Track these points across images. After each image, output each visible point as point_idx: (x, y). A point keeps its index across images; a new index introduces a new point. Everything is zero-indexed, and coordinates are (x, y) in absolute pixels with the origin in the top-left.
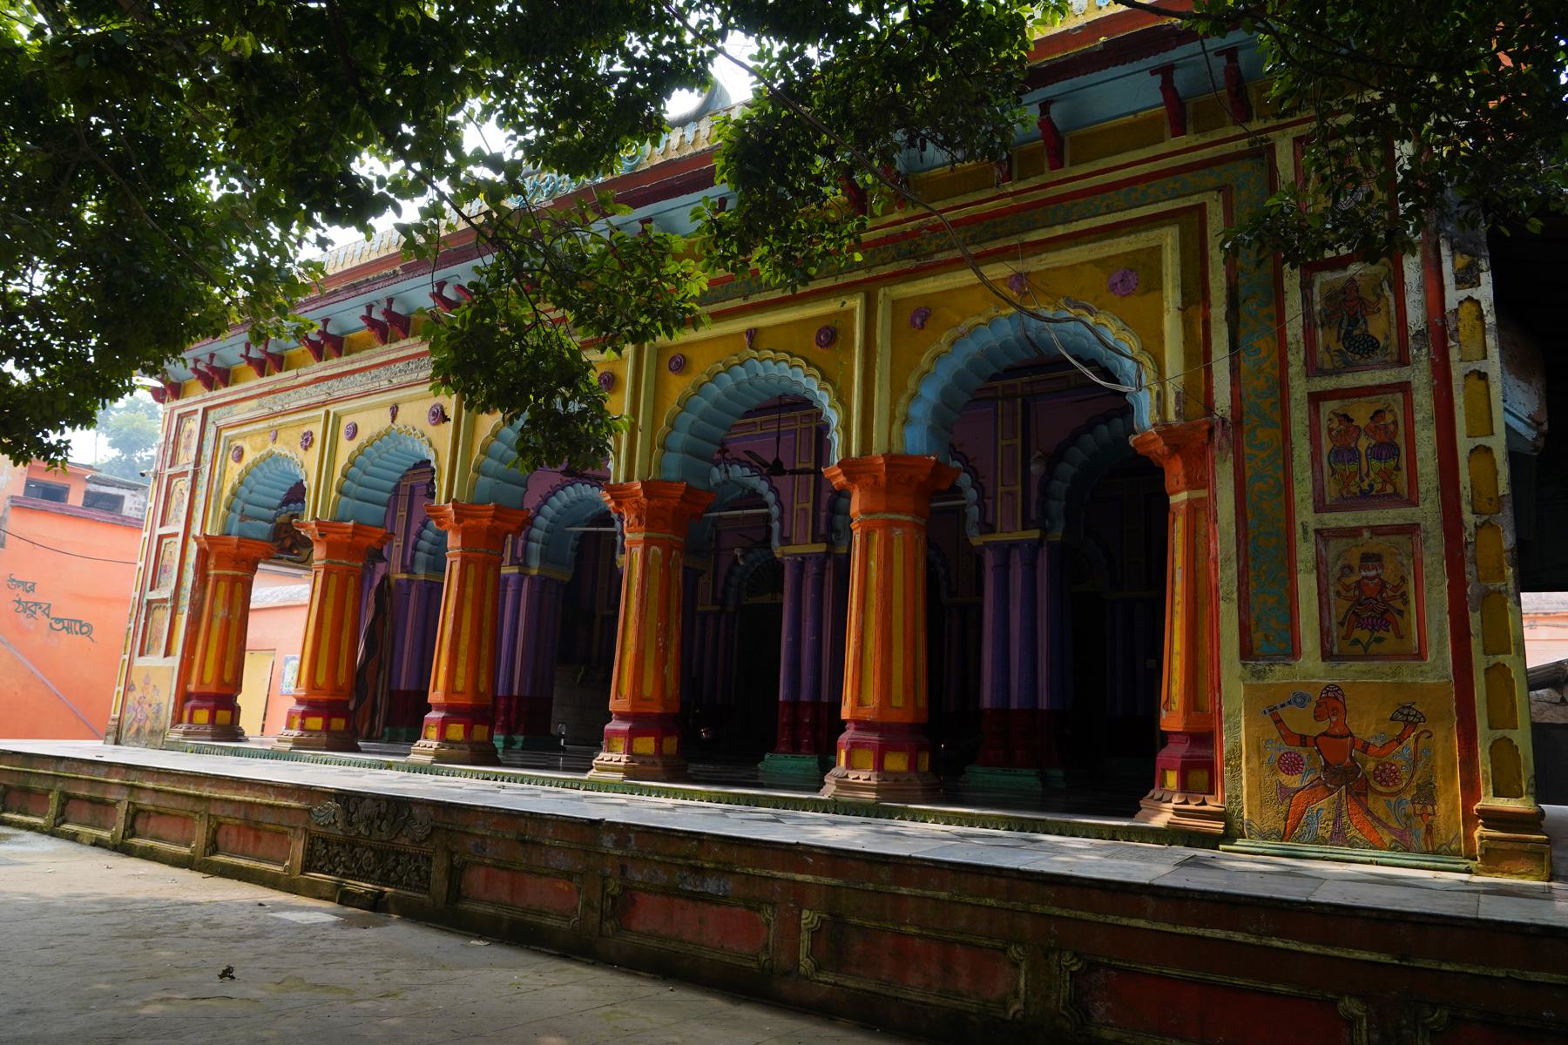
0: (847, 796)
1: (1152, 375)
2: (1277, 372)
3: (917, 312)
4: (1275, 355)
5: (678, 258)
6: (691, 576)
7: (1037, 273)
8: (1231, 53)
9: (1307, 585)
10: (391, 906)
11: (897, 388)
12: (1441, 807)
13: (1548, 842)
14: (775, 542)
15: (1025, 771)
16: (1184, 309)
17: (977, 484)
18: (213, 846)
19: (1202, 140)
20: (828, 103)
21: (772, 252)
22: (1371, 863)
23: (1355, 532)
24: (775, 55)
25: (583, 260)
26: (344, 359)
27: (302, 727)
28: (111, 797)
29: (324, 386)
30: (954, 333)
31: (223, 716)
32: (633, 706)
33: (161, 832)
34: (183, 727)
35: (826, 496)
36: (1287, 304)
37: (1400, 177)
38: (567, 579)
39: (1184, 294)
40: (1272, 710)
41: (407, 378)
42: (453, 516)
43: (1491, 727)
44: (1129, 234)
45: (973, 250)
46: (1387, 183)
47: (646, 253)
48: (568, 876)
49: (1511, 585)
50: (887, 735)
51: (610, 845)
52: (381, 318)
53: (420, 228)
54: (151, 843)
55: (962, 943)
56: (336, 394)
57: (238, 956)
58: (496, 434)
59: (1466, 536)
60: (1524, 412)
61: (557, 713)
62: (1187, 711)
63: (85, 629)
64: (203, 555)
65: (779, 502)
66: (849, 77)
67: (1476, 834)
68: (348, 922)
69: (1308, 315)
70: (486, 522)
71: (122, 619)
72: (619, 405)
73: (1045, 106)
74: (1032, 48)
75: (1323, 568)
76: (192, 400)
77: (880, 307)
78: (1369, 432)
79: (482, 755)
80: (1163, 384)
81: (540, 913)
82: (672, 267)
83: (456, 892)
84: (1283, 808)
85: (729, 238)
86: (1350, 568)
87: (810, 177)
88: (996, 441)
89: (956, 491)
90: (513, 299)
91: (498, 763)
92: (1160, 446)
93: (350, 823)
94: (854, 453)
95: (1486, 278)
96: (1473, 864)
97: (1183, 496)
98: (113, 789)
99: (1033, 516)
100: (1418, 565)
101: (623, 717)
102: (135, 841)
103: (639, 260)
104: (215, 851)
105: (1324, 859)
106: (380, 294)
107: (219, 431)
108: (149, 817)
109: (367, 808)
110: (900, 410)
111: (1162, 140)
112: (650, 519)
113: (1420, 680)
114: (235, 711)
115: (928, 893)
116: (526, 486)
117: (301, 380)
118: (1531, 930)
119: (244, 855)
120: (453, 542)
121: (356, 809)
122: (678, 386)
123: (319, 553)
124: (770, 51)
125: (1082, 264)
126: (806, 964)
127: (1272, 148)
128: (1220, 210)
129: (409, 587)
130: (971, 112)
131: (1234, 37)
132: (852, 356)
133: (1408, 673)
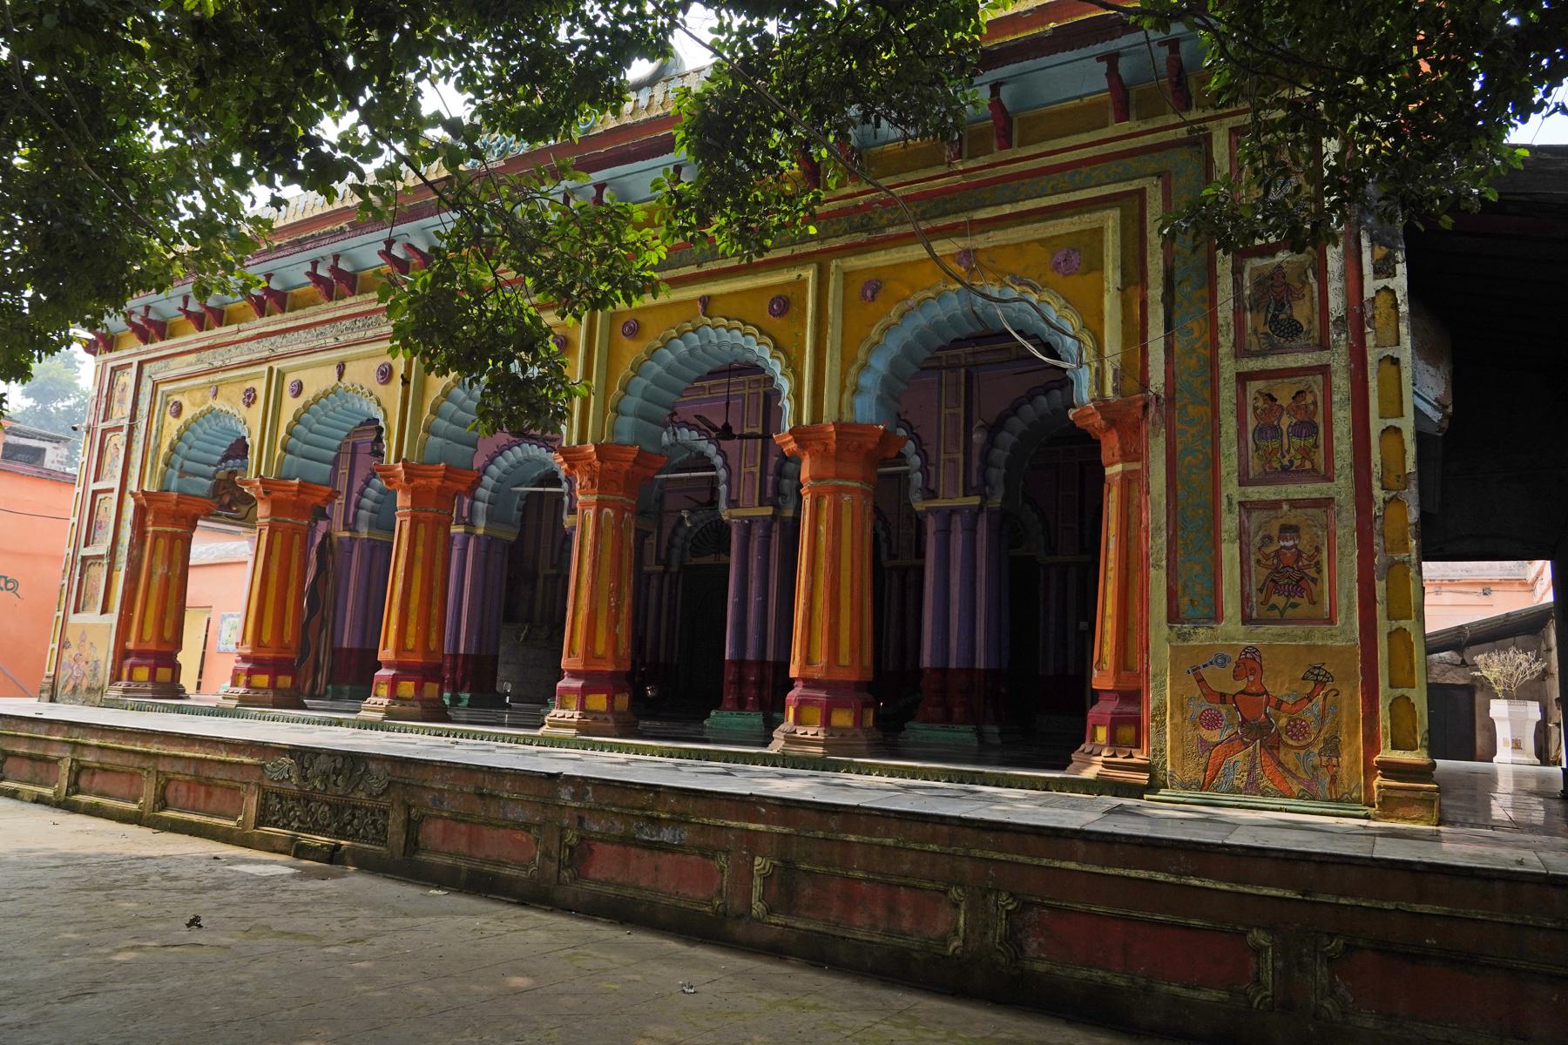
0: (796, 750)
1: (1092, 352)
2: (1207, 353)
3: (868, 284)
4: (1207, 337)
5: (638, 227)
6: (641, 536)
7: (985, 250)
8: (1174, 44)
9: (1230, 552)
10: (348, 859)
11: (847, 360)
12: (1345, 759)
13: (1438, 790)
14: (723, 505)
15: (962, 728)
16: (1122, 290)
17: (921, 451)
18: (162, 802)
19: (1144, 127)
20: (785, 78)
21: (729, 224)
22: (1280, 810)
23: (1275, 505)
24: (735, 29)
25: (543, 227)
26: (289, 315)
27: (248, 684)
28: (53, 754)
29: (266, 342)
30: (904, 306)
31: (164, 673)
32: (1117, 682)
33: (106, 789)
34: (123, 684)
35: (773, 460)
36: (1219, 287)
37: (1326, 173)
38: (513, 538)
39: (1123, 275)
40: (1195, 669)
41: (354, 336)
42: (403, 476)
43: (1391, 686)
44: (1072, 215)
45: (923, 226)
46: (1314, 176)
47: (604, 219)
48: (526, 827)
49: (1414, 556)
50: (835, 693)
52: (327, 275)
53: (377, 190)
54: (96, 799)
55: (906, 886)
56: (280, 351)
57: (202, 905)
58: (446, 394)
59: (1375, 510)
60: (1431, 395)
61: (502, 672)
62: (1117, 671)
63: (10, 585)
64: (140, 512)
65: (726, 465)
66: (807, 53)
67: (1375, 784)
68: (306, 874)
69: (1238, 299)
70: (436, 482)
71: (55, 576)
72: (575, 369)
73: (995, 88)
74: (985, 31)
75: (1245, 538)
76: (126, 352)
77: (832, 278)
78: (1292, 411)
79: (435, 712)
80: (1102, 362)
81: (499, 863)
82: (631, 236)
83: (413, 844)
84: (1203, 760)
85: (691, 209)
86: (1270, 538)
87: (767, 151)
88: (939, 412)
89: (901, 458)
90: (473, 263)
91: (449, 720)
92: (1098, 421)
93: (305, 778)
94: (805, 421)
95: (1401, 269)
96: (1371, 811)
97: (1118, 468)
98: (55, 746)
99: (974, 483)
100: (1331, 536)
101: (575, 674)
102: (79, 797)
103: (601, 228)
104: (165, 807)
105: (1238, 807)
106: (326, 250)
107: (155, 385)
108: (93, 774)
109: (322, 764)
110: (850, 380)
111: (1105, 125)
112: (602, 482)
113: (1329, 643)
114: (176, 668)
115: (875, 840)
116: (475, 446)
117: (243, 335)
118: (1418, 868)
119: (194, 810)
120: (403, 501)
121: (311, 764)
122: (631, 351)
123: (262, 510)
124: (729, 24)
125: (1028, 243)
126: (758, 907)
127: (1208, 138)
128: (1159, 195)
129: (352, 546)
130: (926, 93)
131: (1177, 29)
132: (804, 326)
133: (1319, 636)
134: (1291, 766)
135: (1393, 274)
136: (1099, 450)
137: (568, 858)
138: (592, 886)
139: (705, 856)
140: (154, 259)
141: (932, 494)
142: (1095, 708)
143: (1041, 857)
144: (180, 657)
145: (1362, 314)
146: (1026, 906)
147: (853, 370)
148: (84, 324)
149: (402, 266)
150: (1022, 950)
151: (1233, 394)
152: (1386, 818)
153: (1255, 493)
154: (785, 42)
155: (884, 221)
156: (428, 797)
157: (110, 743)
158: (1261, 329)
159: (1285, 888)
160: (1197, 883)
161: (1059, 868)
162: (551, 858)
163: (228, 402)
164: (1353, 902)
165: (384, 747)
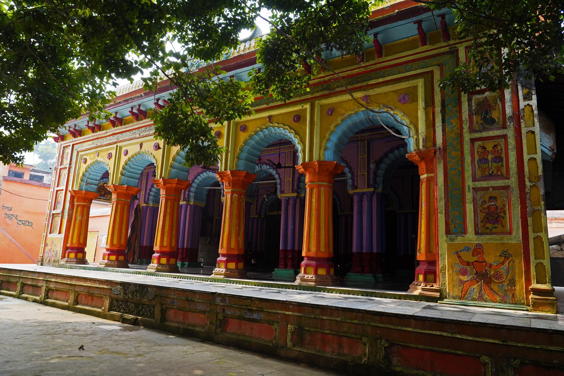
0: (304, 284)
1: (414, 132)
2: (459, 131)
4: (458, 126)
5: (243, 90)
6: (248, 205)
7: (373, 95)
8: (443, 16)
9: (469, 207)
10: (141, 324)
11: (322, 138)
12: (518, 288)
13: (556, 300)
14: (278, 192)
15: (368, 275)
16: (425, 108)
17: (351, 171)
18: (76, 302)
20: (297, 34)
21: (277, 88)
22: (492, 307)
23: (487, 189)
24: (278, 16)
25: (209, 91)
26: (123, 126)
27: (108, 259)
28: (40, 284)
29: (116, 136)
30: (343, 117)
31: (80, 255)
33: (58, 297)
34: (66, 259)
36: (463, 106)
37: (504, 61)
38: (203, 206)
40: (457, 253)
41: (146, 134)
43: (535, 259)
44: (406, 81)
46: (499, 63)
47: (231, 88)
48: (204, 312)
49: (543, 208)
50: (318, 262)
51: (219, 301)
52: (136, 112)
53: (150, 79)
55: (345, 336)
56: (120, 139)
57: (85, 341)
58: (178, 153)
59: (527, 190)
61: (200, 254)
62: (426, 253)
63: (30, 224)
64: (72, 197)
65: (280, 178)
66: (305, 24)
67: (530, 297)
68: (125, 329)
69: (470, 110)
70: (174, 185)
71: (44, 221)
72: (222, 143)
73: (376, 35)
74: (371, 14)
75: (475, 202)
76: (68, 141)
77: (316, 107)
78: (492, 153)
79: (173, 269)
80: (418, 136)
81: (194, 326)
82: (241, 93)
83: (163, 318)
84: (461, 288)
85: (262, 83)
86: (485, 202)
89: (343, 174)
91: (179, 272)
92: (417, 158)
93: (126, 294)
95: (534, 97)
96: (529, 308)
97: (425, 176)
98: (40, 282)
99: (371, 183)
101: (223, 255)
103: (229, 90)
104: (77, 304)
105: (475, 306)
106: (136, 103)
107: (78, 152)
109: (132, 288)
110: (323, 145)
112: (233, 184)
113: (510, 242)
114: (84, 253)
115: (333, 318)
116: (188, 172)
119: (87, 305)
120: (163, 192)
121: (128, 288)
122: (243, 136)
123: (114, 196)
124: (276, 15)
125: (389, 92)
126: (289, 344)
127: (457, 50)
129: (147, 209)
130: (349, 37)
132: (306, 126)
133: (506, 239)
134: (496, 290)
135: (531, 99)
136: (418, 170)
137: (215, 324)
138: (228, 335)
139: (270, 324)
140: (75, 108)
141: (355, 187)
143: (397, 326)
144: (86, 249)
145: (519, 115)
146: (392, 345)
147: (324, 141)
148: (51, 131)
149: (161, 107)
150: (391, 363)
151: (469, 146)
152: (535, 311)
153: (479, 184)
154: (296, 21)
155: (335, 86)
156: (169, 301)
157: (59, 280)
158: (479, 122)
159: (495, 339)
160: (460, 337)
161: (405, 330)
162: (213, 324)
163: (103, 158)
164: (523, 345)
165: (154, 282)
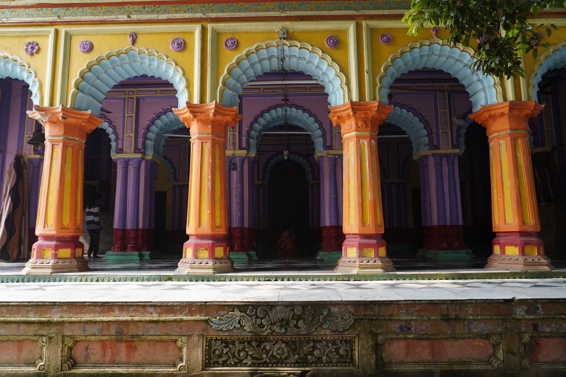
15: (461, 251)
32: (376, 230)
50: (62, 242)
99: (455, 143)
109: (274, 315)
119: (113, 363)
122: (388, 54)
138: (544, 367)
142: (187, 242)
